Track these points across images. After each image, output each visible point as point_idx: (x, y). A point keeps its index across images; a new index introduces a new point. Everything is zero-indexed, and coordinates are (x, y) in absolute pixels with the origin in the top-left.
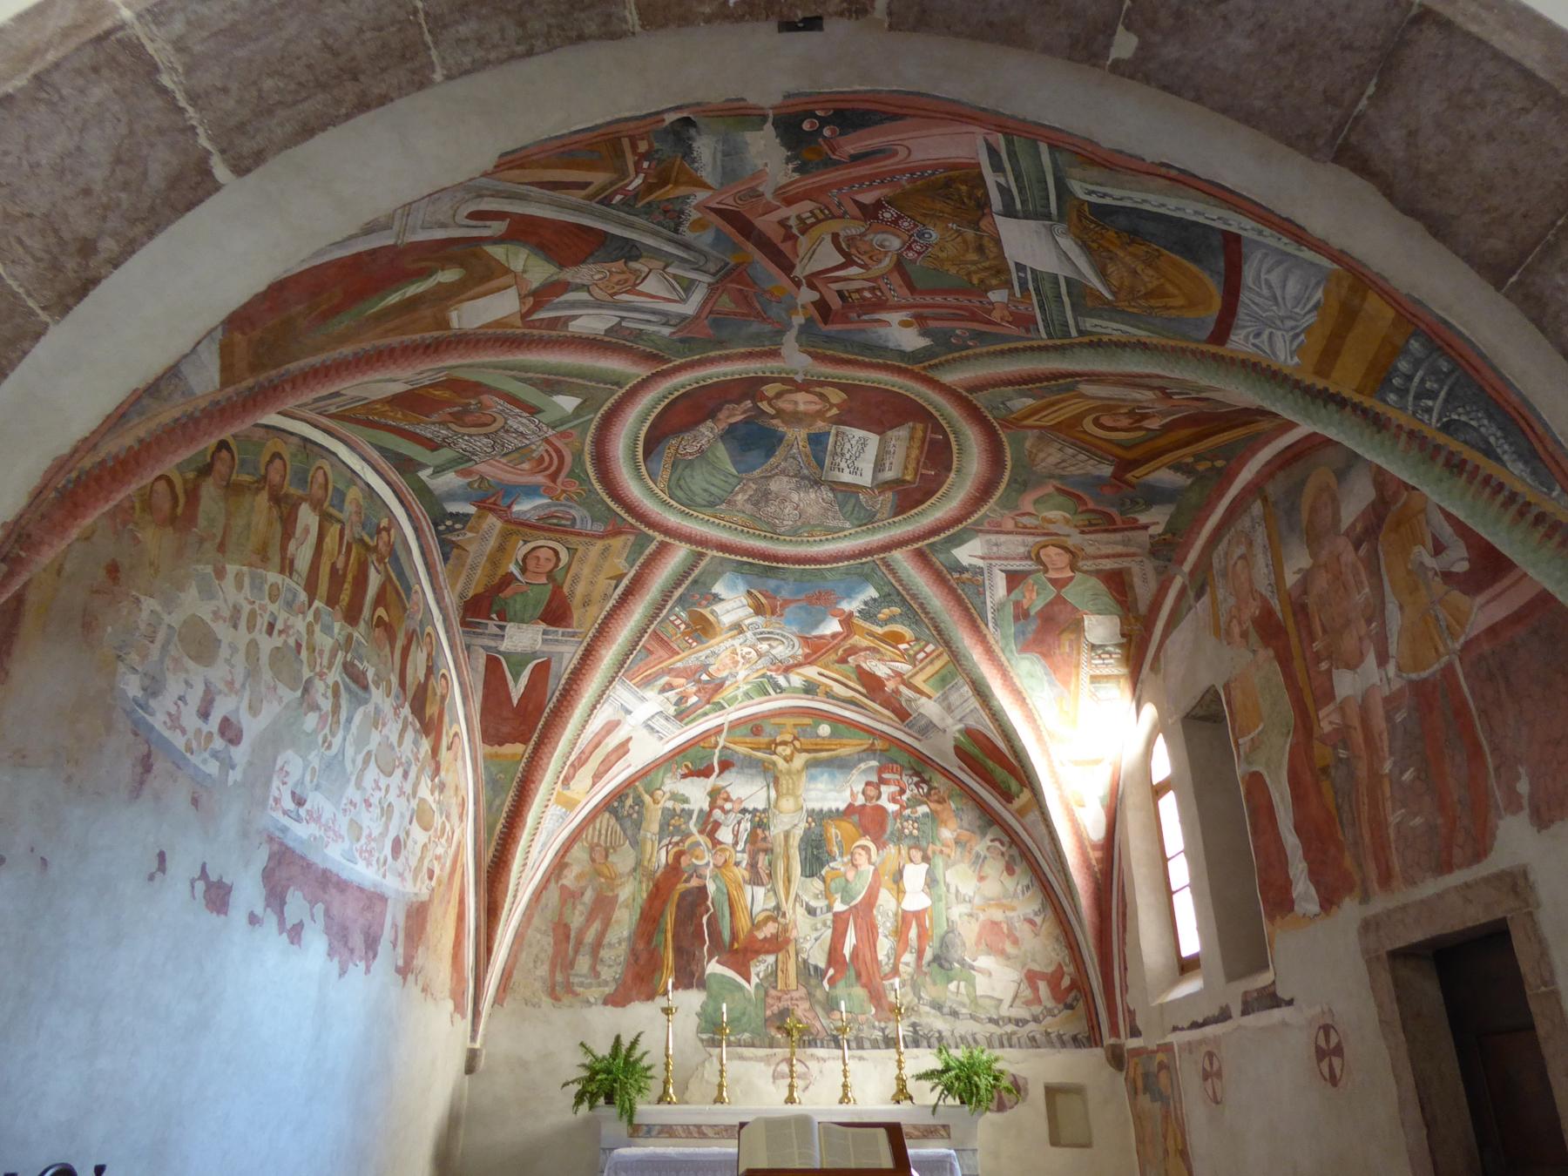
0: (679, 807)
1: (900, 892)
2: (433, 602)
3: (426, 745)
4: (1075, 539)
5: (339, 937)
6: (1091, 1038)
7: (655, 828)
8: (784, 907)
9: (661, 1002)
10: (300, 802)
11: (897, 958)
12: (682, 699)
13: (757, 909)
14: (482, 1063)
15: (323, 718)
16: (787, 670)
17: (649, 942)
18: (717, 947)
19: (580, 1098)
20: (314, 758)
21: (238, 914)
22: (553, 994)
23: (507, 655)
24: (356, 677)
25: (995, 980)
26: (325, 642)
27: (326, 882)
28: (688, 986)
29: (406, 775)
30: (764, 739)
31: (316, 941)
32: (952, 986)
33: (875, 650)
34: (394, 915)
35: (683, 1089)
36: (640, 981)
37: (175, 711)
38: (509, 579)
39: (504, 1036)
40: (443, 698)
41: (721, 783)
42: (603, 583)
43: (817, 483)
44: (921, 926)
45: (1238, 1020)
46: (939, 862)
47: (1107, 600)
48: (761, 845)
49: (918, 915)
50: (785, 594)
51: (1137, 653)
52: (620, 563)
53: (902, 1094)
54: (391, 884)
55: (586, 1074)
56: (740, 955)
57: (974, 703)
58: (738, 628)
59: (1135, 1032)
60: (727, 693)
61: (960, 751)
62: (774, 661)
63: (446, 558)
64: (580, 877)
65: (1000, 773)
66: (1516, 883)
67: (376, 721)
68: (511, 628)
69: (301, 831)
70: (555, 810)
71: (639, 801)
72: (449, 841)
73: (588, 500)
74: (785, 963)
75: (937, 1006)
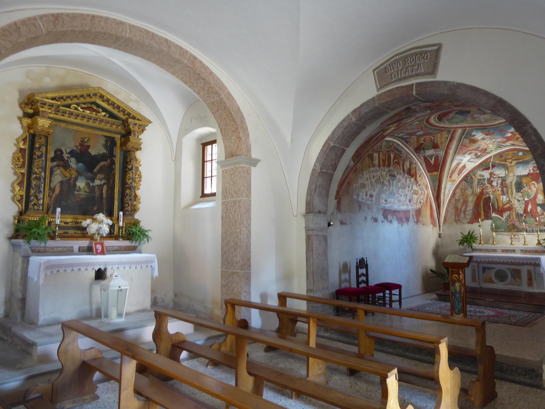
0: (482, 178)
2: (408, 150)
3: (413, 179)
5: (400, 221)
7: (476, 183)
8: (511, 200)
10: (386, 201)
13: (504, 201)
15: (387, 186)
18: (494, 210)
19: (460, 243)
20: (387, 193)
22: (456, 221)
23: (428, 156)
26: (384, 173)
27: (395, 212)
28: (488, 219)
29: (409, 187)
30: (503, 158)
31: (395, 223)
36: (475, 218)
37: (362, 197)
38: (422, 144)
39: (446, 230)
40: (416, 168)
41: (492, 171)
48: (504, 185)
52: (446, 136)
53: (539, 243)
54: (410, 208)
62: (498, 142)
64: (459, 196)
67: (399, 181)
68: (426, 151)
70: (449, 184)
71: (471, 178)
72: (424, 195)
74: (512, 213)
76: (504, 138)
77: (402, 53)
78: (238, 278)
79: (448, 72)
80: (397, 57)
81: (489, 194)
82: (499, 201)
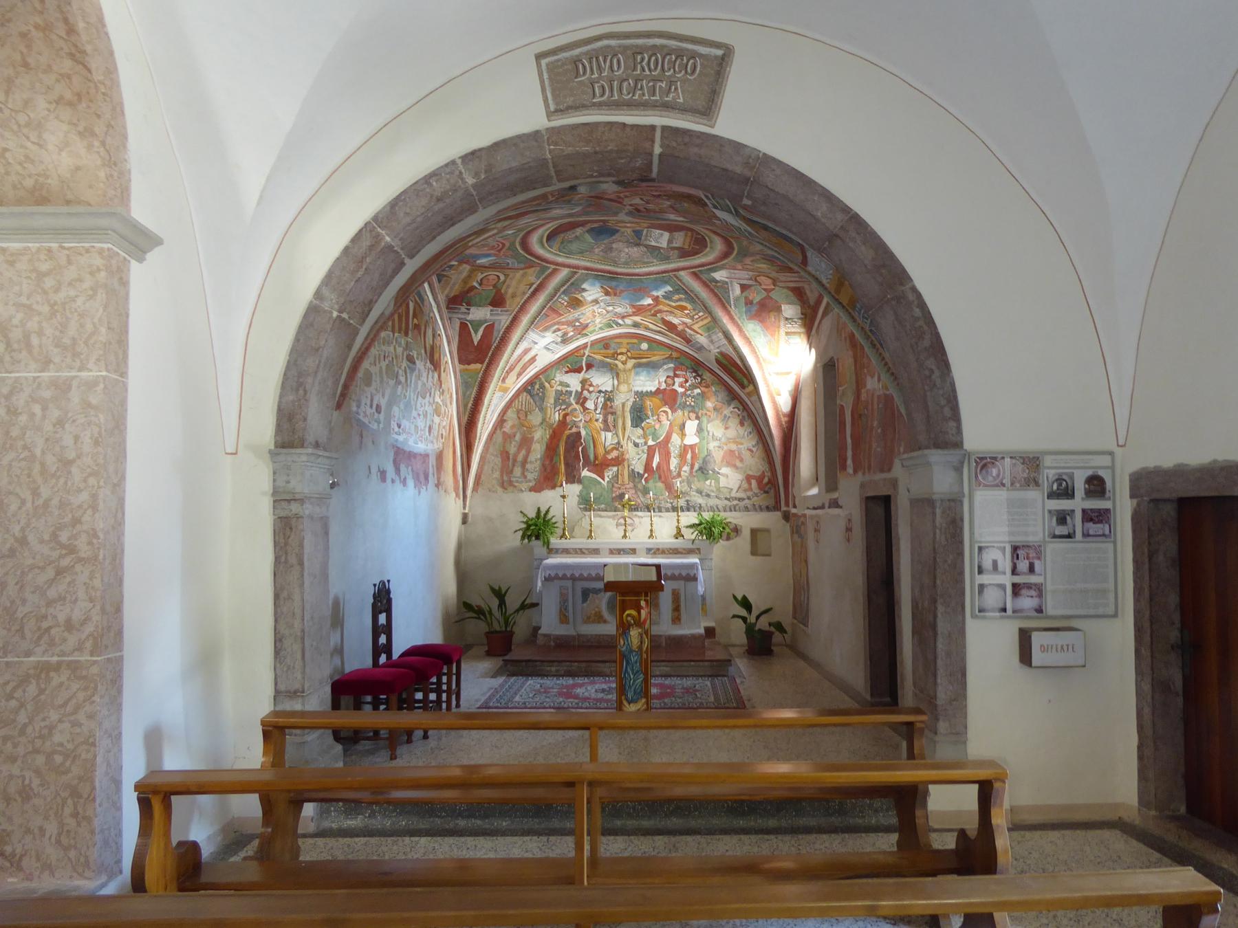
0: (564, 389)
1: (683, 435)
3: (436, 375)
4: (774, 274)
6: (776, 507)
7: (552, 401)
9: (559, 491)
10: (399, 426)
11: (680, 469)
12: (565, 334)
14: (470, 519)
16: (623, 317)
17: (552, 460)
18: (587, 463)
21: (389, 480)
22: (503, 486)
23: (471, 322)
24: (411, 360)
25: (730, 479)
27: (411, 456)
28: (573, 482)
32: (708, 482)
33: (671, 312)
34: (432, 461)
35: (572, 530)
36: (548, 479)
38: (473, 288)
39: (479, 506)
42: (522, 287)
43: (638, 245)
44: (693, 452)
45: (827, 510)
46: (705, 419)
47: (793, 298)
49: (692, 447)
50: (621, 288)
51: (809, 322)
52: (532, 279)
53: (679, 534)
55: (524, 526)
56: (599, 467)
57: (724, 341)
58: (596, 301)
59: (795, 507)
60: (590, 329)
61: (718, 361)
62: (616, 314)
63: (439, 281)
64: (513, 427)
65: (738, 374)
66: (894, 483)
68: (473, 309)
69: (401, 438)
70: (498, 394)
71: (542, 387)
73: (516, 256)
75: (700, 492)
76: (633, 306)
77: (628, 35)
78: (75, 686)
79: (751, 119)
80: (613, 42)
81: (578, 427)
82: (598, 443)
